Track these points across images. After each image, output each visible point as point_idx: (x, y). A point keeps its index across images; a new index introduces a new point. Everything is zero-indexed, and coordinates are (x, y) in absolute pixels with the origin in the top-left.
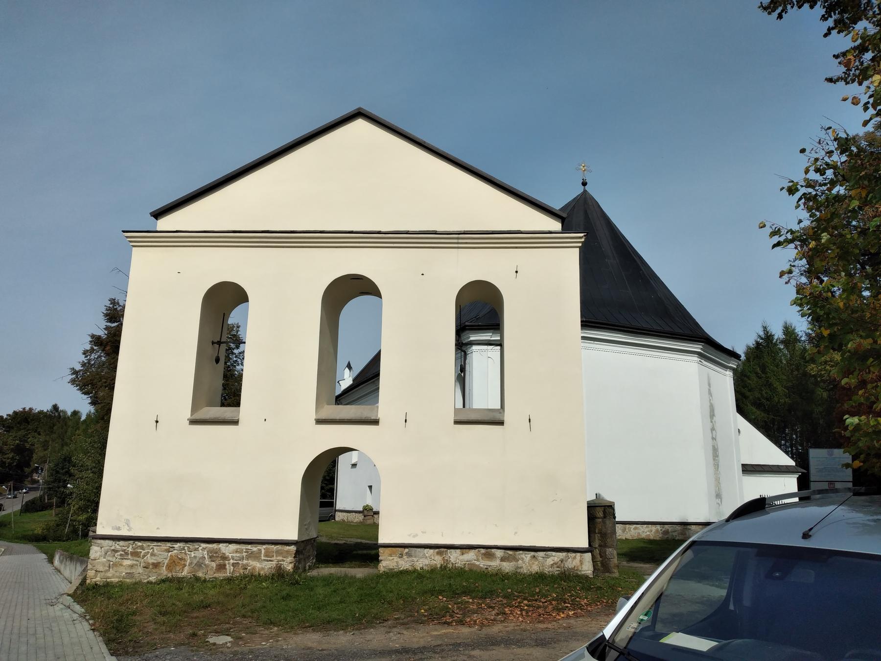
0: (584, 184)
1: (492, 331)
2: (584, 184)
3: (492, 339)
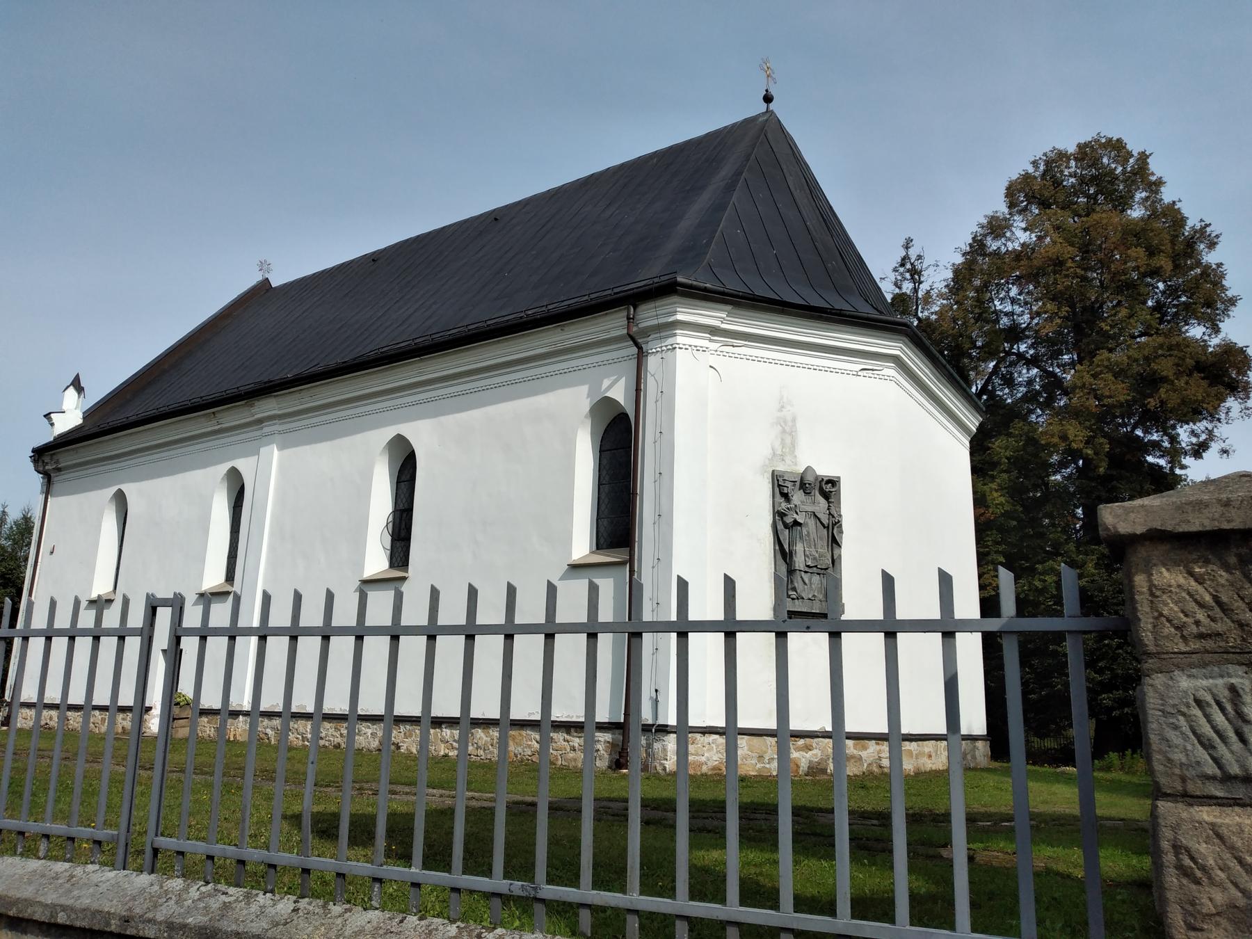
0: (768, 99)
1: (729, 308)
2: (768, 99)
3: (724, 326)
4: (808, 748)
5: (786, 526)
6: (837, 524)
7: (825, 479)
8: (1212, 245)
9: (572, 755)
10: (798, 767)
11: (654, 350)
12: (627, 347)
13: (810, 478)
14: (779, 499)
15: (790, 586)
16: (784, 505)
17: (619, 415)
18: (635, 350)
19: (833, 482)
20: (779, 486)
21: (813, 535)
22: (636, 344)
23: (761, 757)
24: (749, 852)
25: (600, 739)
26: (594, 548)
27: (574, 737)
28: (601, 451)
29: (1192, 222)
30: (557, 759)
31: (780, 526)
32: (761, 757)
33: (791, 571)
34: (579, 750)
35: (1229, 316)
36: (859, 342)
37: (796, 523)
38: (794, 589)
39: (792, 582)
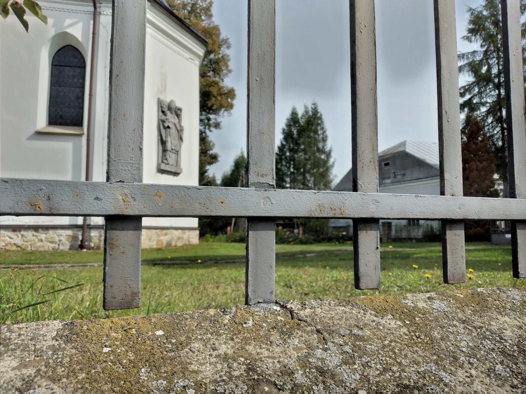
4: (166, 234)
5: (165, 128)
6: (182, 130)
7: (178, 108)
8: (228, 47)
9: (40, 244)
10: (163, 243)
11: (105, 13)
12: (87, 6)
13: (173, 106)
14: (161, 114)
15: (164, 158)
16: (163, 117)
17: (67, 46)
18: (92, 9)
19: (180, 110)
20: (162, 107)
21: (174, 135)
22: (95, 6)
23: (150, 239)
24: (338, 277)
25: (62, 234)
26: (48, 124)
27: (41, 233)
28: (52, 65)
29: (223, 36)
30: (27, 247)
31: (162, 127)
32: (150, 239)
33: (165, 150)
34: (45, 241)
35: (228, 76)
36: (190, 44)
37: (168, 127)
38: (166, 159)
39: (165, 156)
